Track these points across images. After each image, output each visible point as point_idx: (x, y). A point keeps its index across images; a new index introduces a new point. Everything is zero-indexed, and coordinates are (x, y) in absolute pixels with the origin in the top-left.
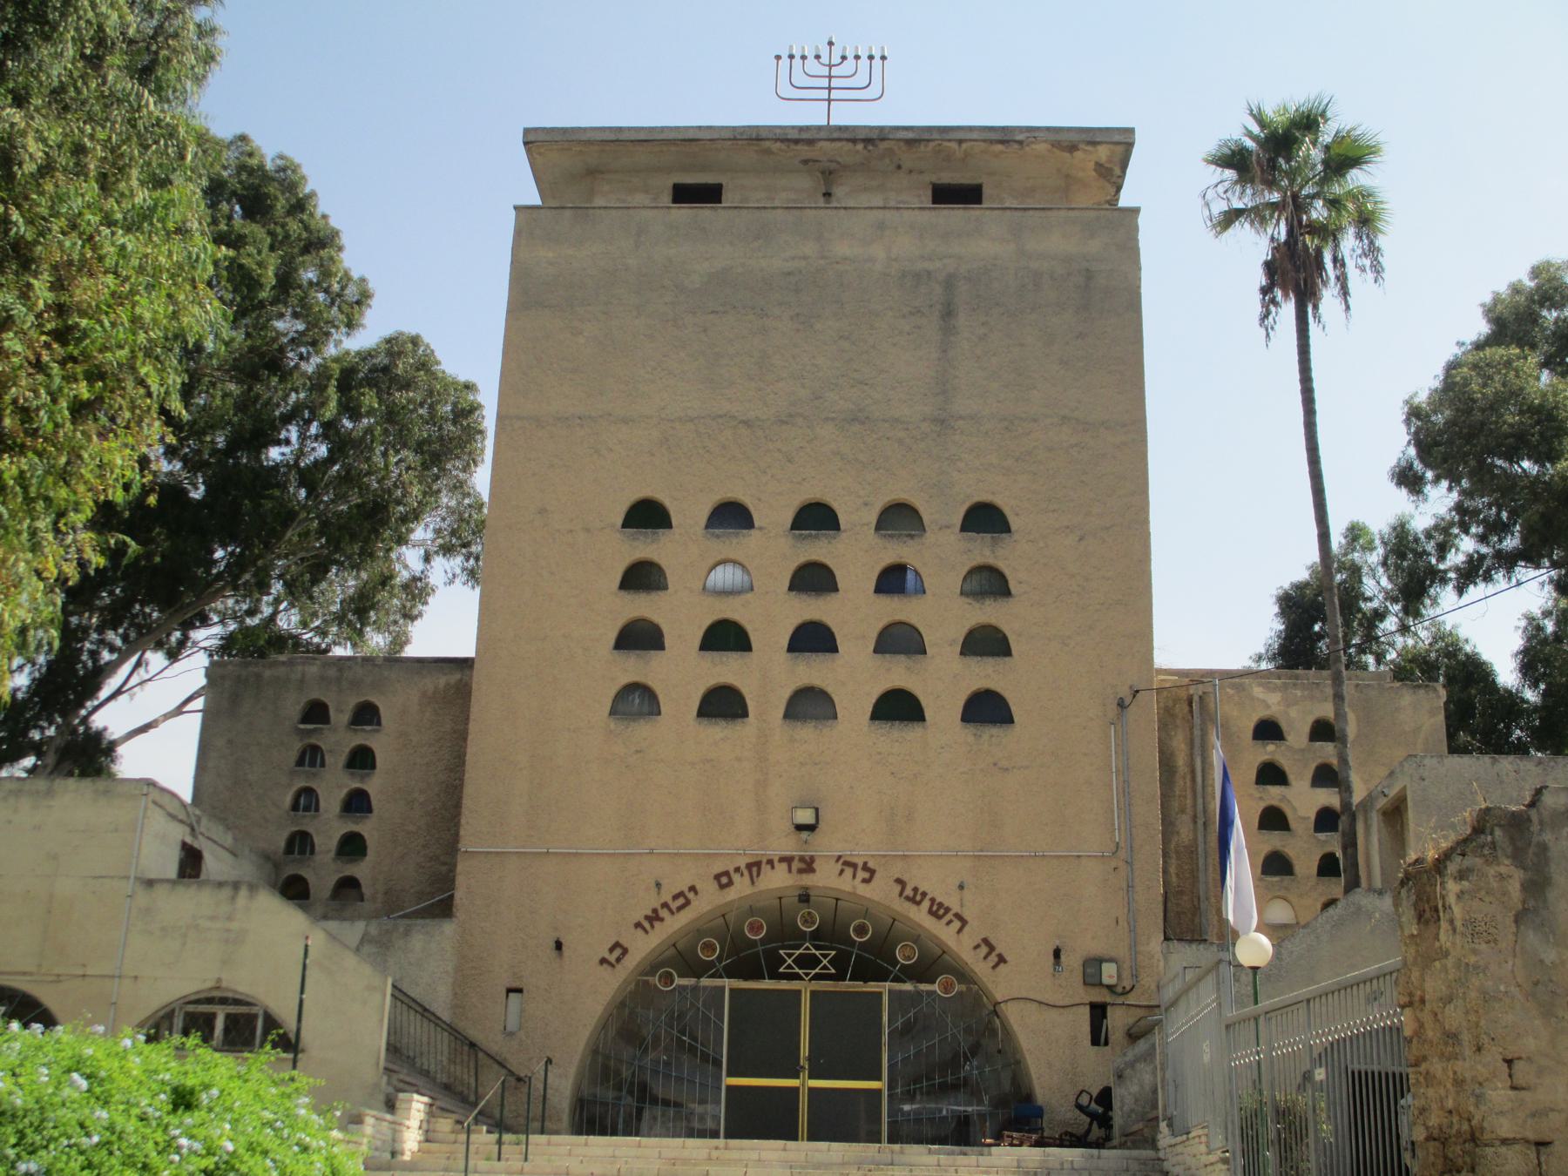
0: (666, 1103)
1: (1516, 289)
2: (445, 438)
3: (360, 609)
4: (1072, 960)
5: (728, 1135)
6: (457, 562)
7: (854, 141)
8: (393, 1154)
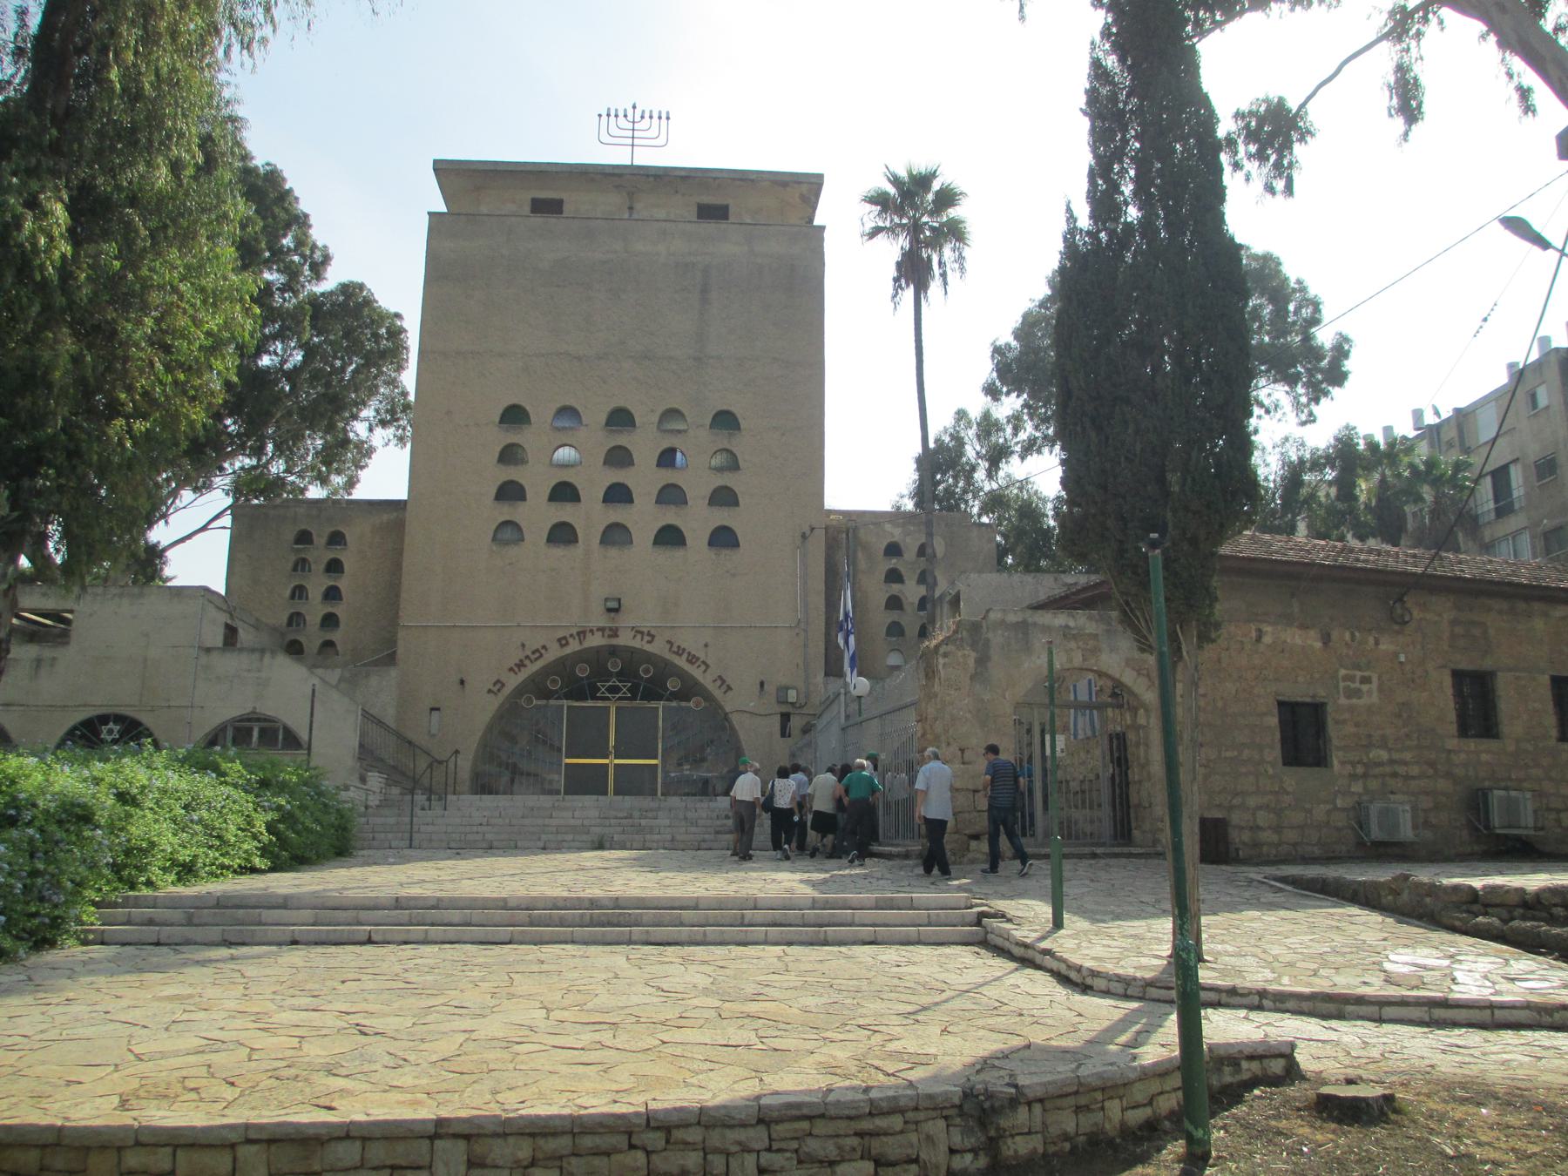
0: (529, 774)
4: (770, 688)
5: (566, 793)
6: (390, 431)
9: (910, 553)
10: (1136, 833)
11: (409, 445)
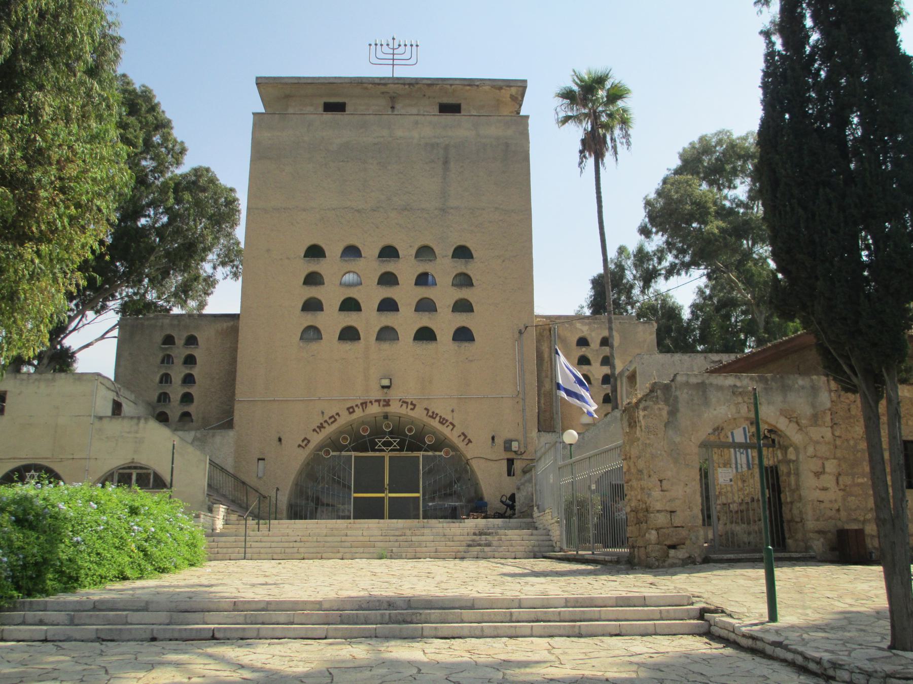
0: (328, 505)
1: (692, 144)
2: (222, 212)
3: (185, 291)
6: (228, 269)
7: (404, 84)
8: (213, 530)
9: (595, 343)
10: (790, 542)
11: (240, 279)
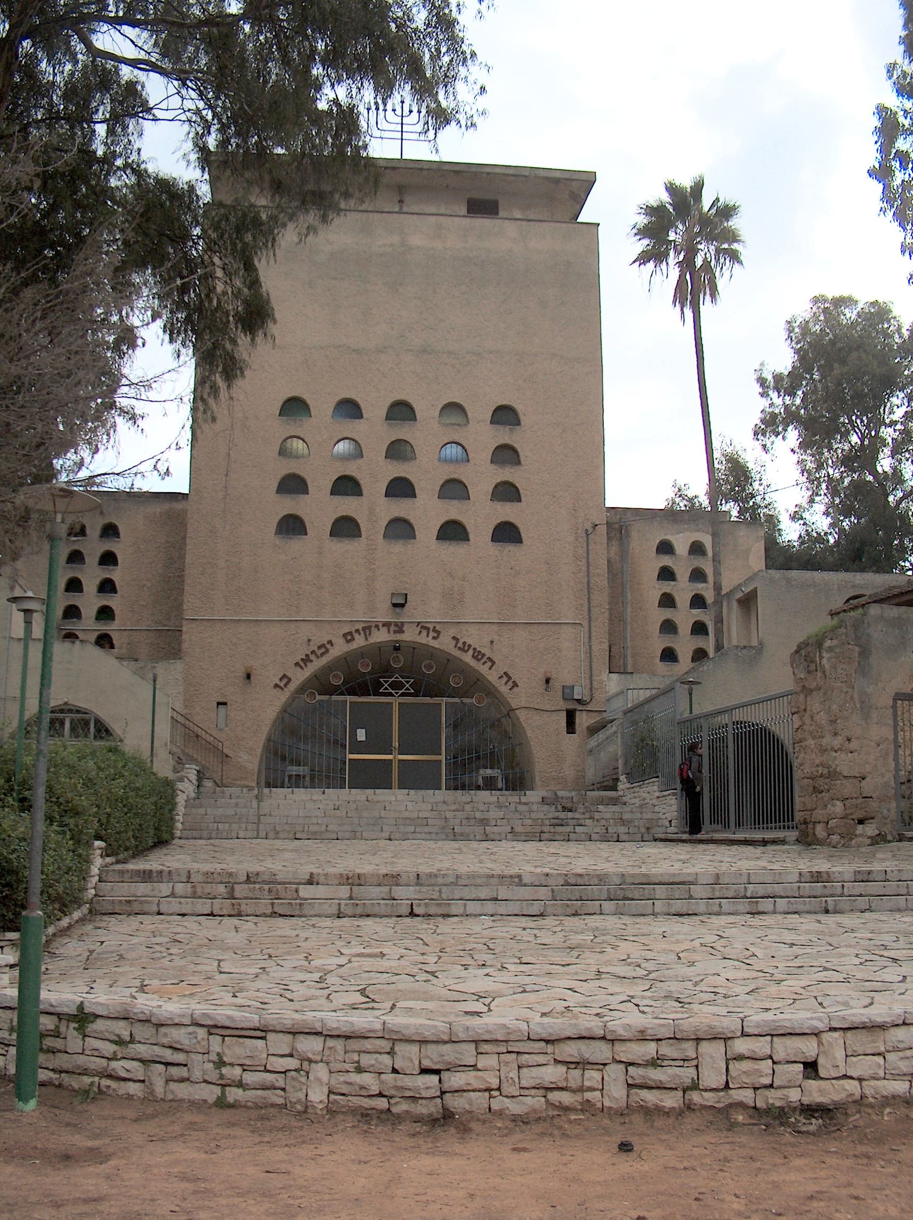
4: (557, 685)
